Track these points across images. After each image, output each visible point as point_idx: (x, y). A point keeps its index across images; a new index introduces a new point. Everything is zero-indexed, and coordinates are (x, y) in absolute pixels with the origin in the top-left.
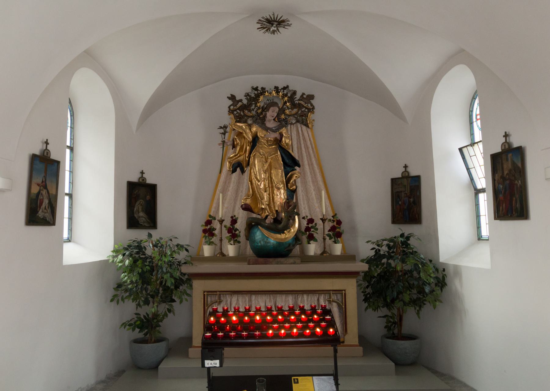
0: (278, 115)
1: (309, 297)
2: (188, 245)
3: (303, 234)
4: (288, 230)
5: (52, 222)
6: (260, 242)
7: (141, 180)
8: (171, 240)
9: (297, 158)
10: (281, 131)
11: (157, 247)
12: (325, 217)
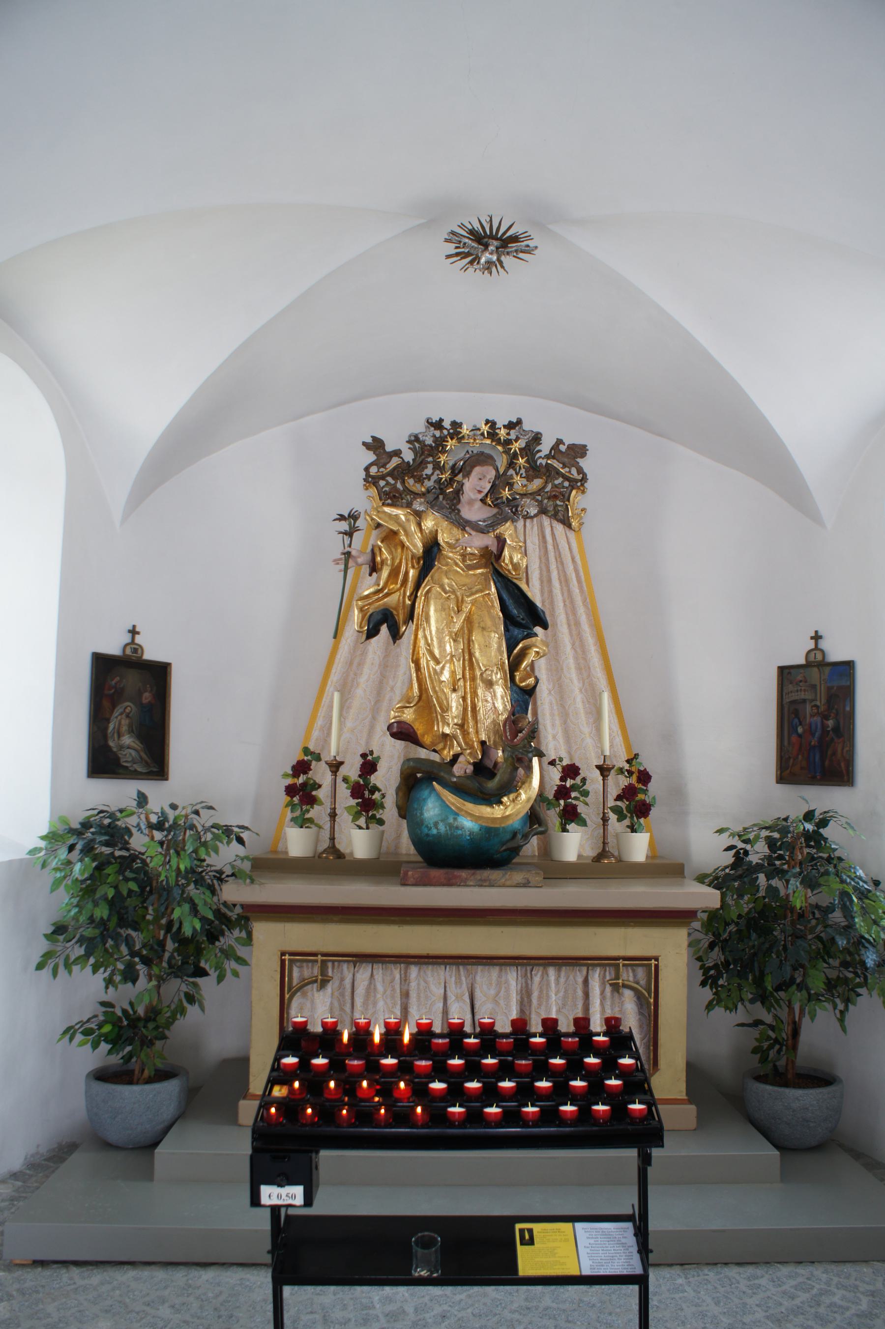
1: (563, 974)
3: (549, 803)
4: (512, 796)
6: (436, 824)
8: (197, 813)
9: (539, 604)
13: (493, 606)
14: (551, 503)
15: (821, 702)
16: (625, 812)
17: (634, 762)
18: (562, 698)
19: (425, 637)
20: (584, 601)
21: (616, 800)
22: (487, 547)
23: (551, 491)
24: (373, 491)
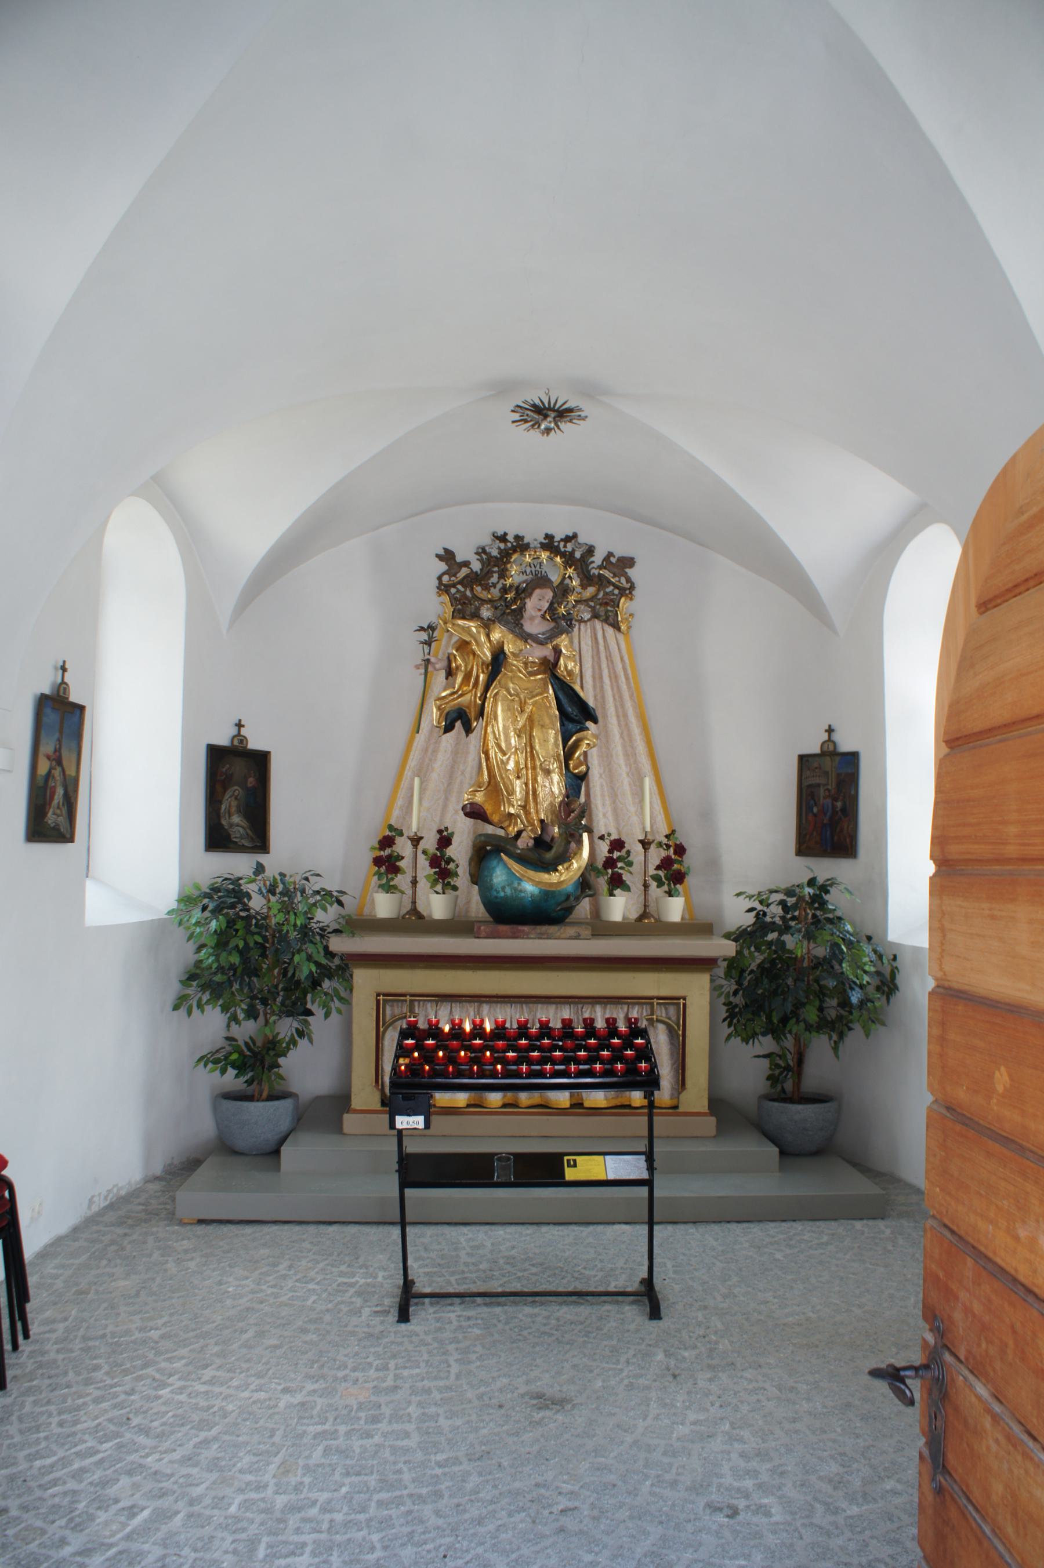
0: (551, 609)
2: (338, 892)
4: (566, 865)
5: (68, 836)
6: (503, 888)
7: (236, 743)
8: (307, 879)
9: (591, 703)
11: (274, 894)
12: (650, 837)
14: (602, 609)
15: (832, 786)
18: (612, 782)
20: (631, 696)
23: (603, 598)
24: (446, 598)
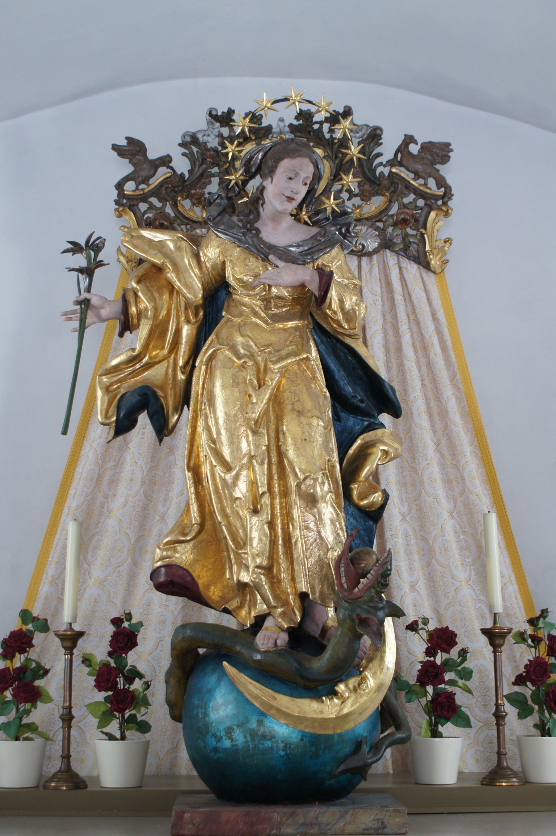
4: (353, 682)
6: (229, 731)
9: (383, 374)
10: (323, 260)
13: (314, 378)
14: (398, 232)
16: (530, 702)
17: (541, 624)
18: (423, 527)
19: (208, 429)
20: (453, 378)
21: (514, 684)
22: (303, 286)
23: (397, 214)
